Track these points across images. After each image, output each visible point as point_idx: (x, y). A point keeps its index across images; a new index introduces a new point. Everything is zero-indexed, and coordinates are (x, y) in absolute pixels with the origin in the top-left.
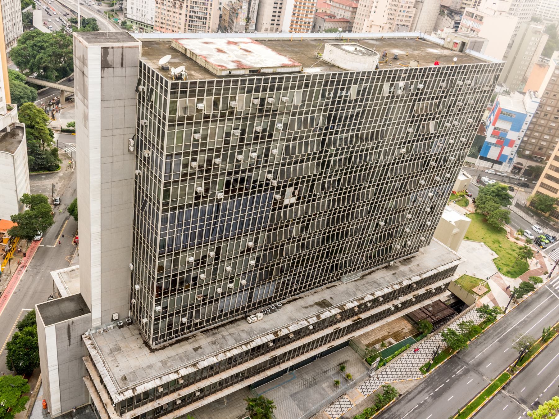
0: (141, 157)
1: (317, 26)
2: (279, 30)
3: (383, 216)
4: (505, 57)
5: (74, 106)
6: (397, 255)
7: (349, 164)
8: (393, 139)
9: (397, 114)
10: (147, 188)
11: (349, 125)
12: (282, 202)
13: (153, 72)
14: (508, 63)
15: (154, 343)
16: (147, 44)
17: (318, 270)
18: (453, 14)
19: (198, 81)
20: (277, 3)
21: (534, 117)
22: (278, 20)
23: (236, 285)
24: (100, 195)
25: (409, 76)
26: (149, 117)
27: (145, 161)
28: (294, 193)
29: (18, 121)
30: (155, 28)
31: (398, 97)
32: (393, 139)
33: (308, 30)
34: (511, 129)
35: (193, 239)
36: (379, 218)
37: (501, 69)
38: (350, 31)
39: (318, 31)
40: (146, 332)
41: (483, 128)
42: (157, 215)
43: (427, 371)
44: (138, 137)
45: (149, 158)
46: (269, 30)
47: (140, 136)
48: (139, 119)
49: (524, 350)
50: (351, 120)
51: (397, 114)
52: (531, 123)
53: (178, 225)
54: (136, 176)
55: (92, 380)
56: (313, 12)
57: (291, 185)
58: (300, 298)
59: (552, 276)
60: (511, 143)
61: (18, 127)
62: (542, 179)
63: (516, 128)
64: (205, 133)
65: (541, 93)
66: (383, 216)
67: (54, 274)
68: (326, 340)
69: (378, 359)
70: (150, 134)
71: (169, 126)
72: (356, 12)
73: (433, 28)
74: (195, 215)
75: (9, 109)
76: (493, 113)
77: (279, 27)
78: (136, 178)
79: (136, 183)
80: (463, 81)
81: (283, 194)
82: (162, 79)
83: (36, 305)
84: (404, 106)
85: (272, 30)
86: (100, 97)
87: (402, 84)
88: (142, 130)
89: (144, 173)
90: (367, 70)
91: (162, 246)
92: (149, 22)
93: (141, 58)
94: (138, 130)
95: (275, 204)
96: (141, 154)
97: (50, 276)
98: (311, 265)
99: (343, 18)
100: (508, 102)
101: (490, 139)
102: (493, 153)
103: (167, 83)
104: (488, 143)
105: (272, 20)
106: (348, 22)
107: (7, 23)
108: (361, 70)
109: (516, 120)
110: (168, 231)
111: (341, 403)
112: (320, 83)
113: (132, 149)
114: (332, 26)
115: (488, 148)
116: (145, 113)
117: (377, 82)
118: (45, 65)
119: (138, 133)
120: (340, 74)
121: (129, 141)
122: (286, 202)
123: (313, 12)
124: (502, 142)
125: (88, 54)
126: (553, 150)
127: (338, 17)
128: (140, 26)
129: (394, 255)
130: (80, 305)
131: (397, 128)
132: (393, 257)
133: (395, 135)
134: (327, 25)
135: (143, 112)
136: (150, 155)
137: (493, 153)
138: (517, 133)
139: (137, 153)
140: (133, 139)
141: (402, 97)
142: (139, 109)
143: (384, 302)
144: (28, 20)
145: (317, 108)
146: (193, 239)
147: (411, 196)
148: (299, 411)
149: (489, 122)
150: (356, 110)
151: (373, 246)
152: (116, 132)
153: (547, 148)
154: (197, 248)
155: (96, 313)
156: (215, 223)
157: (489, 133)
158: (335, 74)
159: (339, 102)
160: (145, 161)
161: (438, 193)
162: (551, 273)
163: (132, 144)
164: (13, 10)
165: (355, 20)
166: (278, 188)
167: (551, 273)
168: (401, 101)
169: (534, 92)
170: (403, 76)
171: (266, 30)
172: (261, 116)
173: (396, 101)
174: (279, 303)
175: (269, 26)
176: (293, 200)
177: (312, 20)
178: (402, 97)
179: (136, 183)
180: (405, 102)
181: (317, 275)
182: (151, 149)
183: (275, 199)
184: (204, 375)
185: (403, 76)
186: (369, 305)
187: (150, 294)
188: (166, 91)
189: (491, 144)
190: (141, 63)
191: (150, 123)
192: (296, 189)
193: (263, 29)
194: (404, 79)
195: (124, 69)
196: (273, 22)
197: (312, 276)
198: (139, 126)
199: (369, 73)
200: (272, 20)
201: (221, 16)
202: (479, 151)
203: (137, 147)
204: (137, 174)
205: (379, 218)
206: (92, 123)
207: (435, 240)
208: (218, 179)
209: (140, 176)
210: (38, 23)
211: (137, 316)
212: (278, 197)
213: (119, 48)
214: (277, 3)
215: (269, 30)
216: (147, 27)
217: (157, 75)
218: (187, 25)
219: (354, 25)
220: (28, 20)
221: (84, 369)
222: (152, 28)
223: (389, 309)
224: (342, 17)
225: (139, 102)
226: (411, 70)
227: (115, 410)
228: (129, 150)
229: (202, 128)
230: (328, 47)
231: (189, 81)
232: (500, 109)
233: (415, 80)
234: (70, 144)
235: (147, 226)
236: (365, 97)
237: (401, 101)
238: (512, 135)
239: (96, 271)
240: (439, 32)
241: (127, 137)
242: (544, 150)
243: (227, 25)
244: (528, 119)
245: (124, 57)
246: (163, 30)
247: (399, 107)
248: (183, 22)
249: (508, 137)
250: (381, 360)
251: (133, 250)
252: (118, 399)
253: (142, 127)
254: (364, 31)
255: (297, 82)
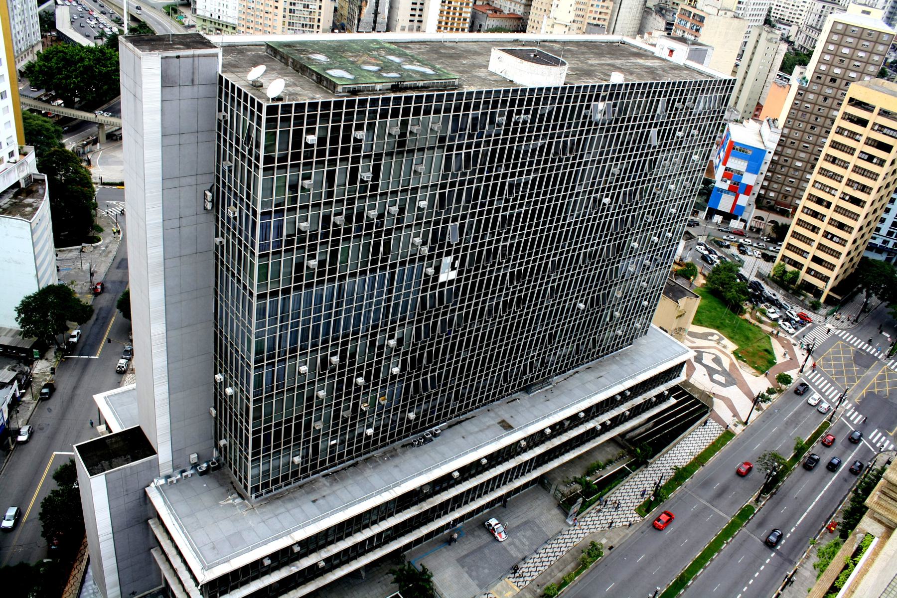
0: (223, 217)
1: (477, 23)
2: (422, 29)
3: (583, 296)
4: (734, 72)
5: (121, 145)
6: (603, 351)
7: (495, 258)
8: (593, 185)
9: (597, 148)
10: (239, 271)
11: (531, 164)
12: (436, 279)
13: (239, 90)
14: (739, 77)
15: (253, 496)
16: (229, 49)
17: (486, 380)
18: (664, 12)
19: (307, 101)
20: (416, 4)
21: (775, 154)
22: (420, 16)
23: (373, 405)
24: (163, 277)
25: (611, 95)
26: (234, 157)
27: (229, 222)
28: (453, 264)
29: (36, 172)
30: (238, 28)
31: (597, 124)
32: (593, 185)
33: (463, 30)
34: (747, 171)
35: (305, 338)
36: (577, 298)
37: (732, 88)
38: (524, 31)
39: (479, 31)
40: (240, 480)
41: (711, 170)
42: (250, 303)
43: (648, 511)
44: (218, 188)
45: (235, 218)
46: (407, 29)
47: (221, 186)
48: (219, 161)
49: (771, 472)
50: (533, 156)
51: (597, 148)
52: (773, 162)
53: (282, 318)
54: (217, 246)
55: (164, 552)
56: (471, 5)
57: (448, 254)
58: (467, 419)
59: (804, 370)
60: (748, 190)
61: (36, 181)
62: (788, 239)
63: (753, 169)
64: (323, 258)
65: (781, 122)
66: (583, 296)
67: (100, 399)
68: (506, 478)
69: (580, 500)
70: (235, 183)
71: (265, 169)
72: (530, 6)
73: (637, 30)
74: (308, 303)
75: (24, 154)
76: (723, 147)
77: (423, 25)
78: (217, 249)
79: (217, 257)
80: (684, 103)
81: (437, 270)
82: (253, 100)
83: (74, 446)
84: (606, 137)
85: (411, 30)
86: (160, 129)
87: (601, 105)
88: (224, 177)
89: (228, 241)
90: (553, 85)
91: (259, 351)
92: (230, 21)
93: (220, 72)
94: (218, 178)
95: (426, 282)
96: (223, 213)
97: (93, 403)
98: (495, 366)
99: (513, 14)
100: (743, 133)
101: (720, 183)
102: (725, 204)
103: (260, 106)
104: (718, 189)
105: (411, 15)
106: (520, 19)
107: (17, 26)
108: (545, 85)
109: (754, 156)
110: (267, 328)
111: (529, 565)
112: (486, 103)
113: (209, 206)
114: (498, 23)
115: (719, 198)
116: (228, 152)
117: (568, 102)
118: (72, 84)
119: (218, 181)
120: (515, 91)
121: (205, 194)
122: (443, 278)
123: (471, 5)
124: (736, 189)
125: (143, 75)
126: (800, 199)
127: (506, 12)
128: (217, 26)
129: (599, 351)
130: (135, 444)
131: (597, 168)
132: (598, 353)
133: (595, 178)
134: (491, 22)
135: (225, 151)
136: (237, 214)
137: (725, 204)
138: (755, 176)
139: (217, 211)
140: (210, 191)
141: (603, 124)
142: (219, 146)
143: (587, 419)
144: (47, 22)
145: (484, 139)
146: (305, 338)
147: (620, 265)
148: (470, 580)
149: (718, 160)
150: (540, 142)
151: (546, 347)
152: (184, 181)
153: (794, 197)
154: (311, 351)
155: (164, 453)
156: (338, 314)
157: (719, 172)
158: (508, 91)
159: (515, 131)
160: (229, 222)
161: (656, 260)
162: (803, 366)
163: (209, 198)
164: (25, 6)
165: (531, 17)
166: (430, 257)
167: (803, 366)
168: (602, 129)
169: (774, 121)
170: (602, 94)
171: (403, 29)
172: (402, 153)
173: (595, 130)
174: (437, 427)
175: (407, 24)
176: (453, 275)
177: (469, 15)
178: (603, 124)
179: (217, 257)
180: (608, 131)
181: (484, 387)
182: (239, 205)
183: (426, 275)
184: (329, 539)
185: (602, 94)
186: (567, 423)
187: (244, 424)
188: (259, 118)
189: (722, 191)
190: (221, 77)
191: (236, 166)
192: (456, 258)
193: (398, 28)
194: (604, 99)
195: (196, 87)
196: (412, 18)
197: (477, 389)
198: (218, 172)
199: (556, 89)
200: (411, 15)
201: (336, 10)
202: (707, 201)
203: (215, 203)
204: (218, 244)
205: (577, 298)
206: (141, 161)
207: (654, 326)
208: (340, 247)
209: (222, 246)
210: (63, 25)
211: (225, 458)
212: (431, 271)
213: (188, 57)
214: (416, 4)
215: (407, 29)
216: (227, 26)
217: (246, 95)
218: (287, 24)
219: (529, 23)
220: (47, 22)
221: (151, 537)
222: (234, 28)
223: (594, 428)
224: (512, 11)
225: (219, 136)
226: (614, 86)
227: (202, 594)
228: (205, 208)
229: (313, 171)
230: (496, 53)
231: (294, 103)
232: (732, 142)
233: (619, 101)
234: (114, 203)
235: (224, 308)
236: (552, 123)
237: (602, 129)
238: (749, 179)
239: (161, 391)
240: (646, 35)
241: (201, 188)
242: (790, 198)
243: (345, 22)
244: (769, 157)
245: (196, 72)
246: (251, 31)
247: (600, 137)
248: (280, 19)
249: (743, 181)
250: (584, 501)
251: (216, 358)
252: (205, 577)
253: (224, 172)
254: (543, 31)
255: (454, 103)
